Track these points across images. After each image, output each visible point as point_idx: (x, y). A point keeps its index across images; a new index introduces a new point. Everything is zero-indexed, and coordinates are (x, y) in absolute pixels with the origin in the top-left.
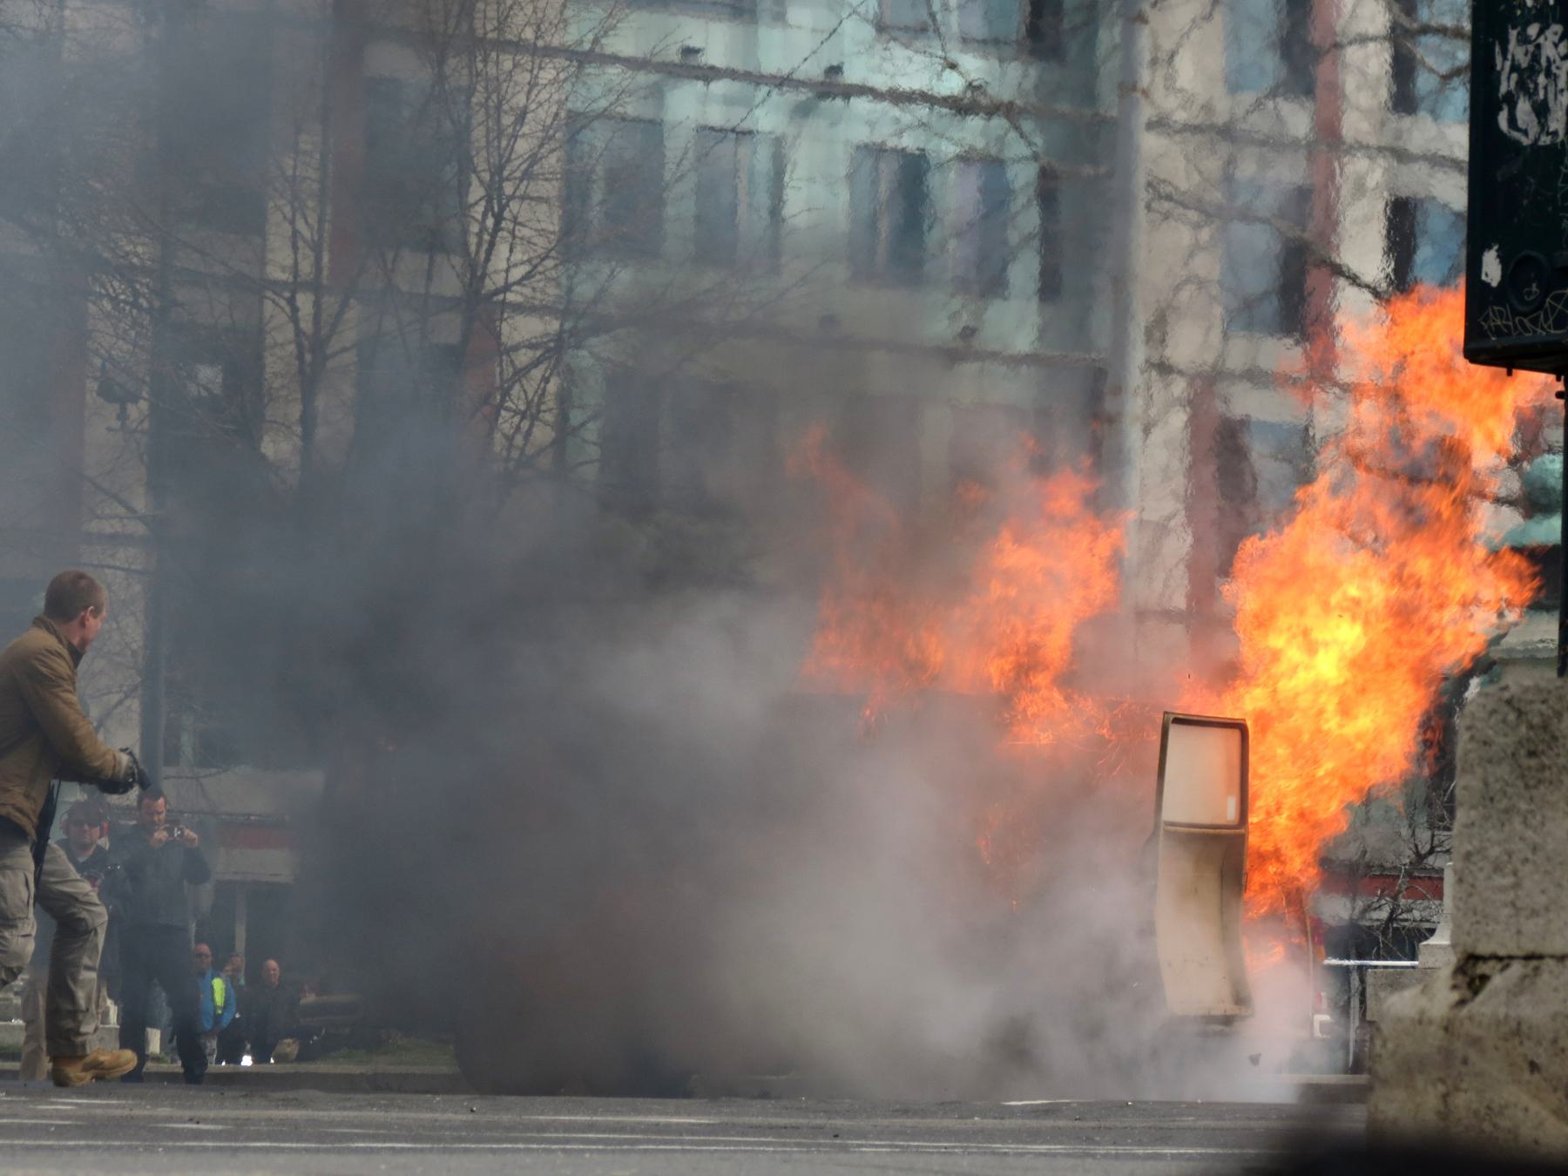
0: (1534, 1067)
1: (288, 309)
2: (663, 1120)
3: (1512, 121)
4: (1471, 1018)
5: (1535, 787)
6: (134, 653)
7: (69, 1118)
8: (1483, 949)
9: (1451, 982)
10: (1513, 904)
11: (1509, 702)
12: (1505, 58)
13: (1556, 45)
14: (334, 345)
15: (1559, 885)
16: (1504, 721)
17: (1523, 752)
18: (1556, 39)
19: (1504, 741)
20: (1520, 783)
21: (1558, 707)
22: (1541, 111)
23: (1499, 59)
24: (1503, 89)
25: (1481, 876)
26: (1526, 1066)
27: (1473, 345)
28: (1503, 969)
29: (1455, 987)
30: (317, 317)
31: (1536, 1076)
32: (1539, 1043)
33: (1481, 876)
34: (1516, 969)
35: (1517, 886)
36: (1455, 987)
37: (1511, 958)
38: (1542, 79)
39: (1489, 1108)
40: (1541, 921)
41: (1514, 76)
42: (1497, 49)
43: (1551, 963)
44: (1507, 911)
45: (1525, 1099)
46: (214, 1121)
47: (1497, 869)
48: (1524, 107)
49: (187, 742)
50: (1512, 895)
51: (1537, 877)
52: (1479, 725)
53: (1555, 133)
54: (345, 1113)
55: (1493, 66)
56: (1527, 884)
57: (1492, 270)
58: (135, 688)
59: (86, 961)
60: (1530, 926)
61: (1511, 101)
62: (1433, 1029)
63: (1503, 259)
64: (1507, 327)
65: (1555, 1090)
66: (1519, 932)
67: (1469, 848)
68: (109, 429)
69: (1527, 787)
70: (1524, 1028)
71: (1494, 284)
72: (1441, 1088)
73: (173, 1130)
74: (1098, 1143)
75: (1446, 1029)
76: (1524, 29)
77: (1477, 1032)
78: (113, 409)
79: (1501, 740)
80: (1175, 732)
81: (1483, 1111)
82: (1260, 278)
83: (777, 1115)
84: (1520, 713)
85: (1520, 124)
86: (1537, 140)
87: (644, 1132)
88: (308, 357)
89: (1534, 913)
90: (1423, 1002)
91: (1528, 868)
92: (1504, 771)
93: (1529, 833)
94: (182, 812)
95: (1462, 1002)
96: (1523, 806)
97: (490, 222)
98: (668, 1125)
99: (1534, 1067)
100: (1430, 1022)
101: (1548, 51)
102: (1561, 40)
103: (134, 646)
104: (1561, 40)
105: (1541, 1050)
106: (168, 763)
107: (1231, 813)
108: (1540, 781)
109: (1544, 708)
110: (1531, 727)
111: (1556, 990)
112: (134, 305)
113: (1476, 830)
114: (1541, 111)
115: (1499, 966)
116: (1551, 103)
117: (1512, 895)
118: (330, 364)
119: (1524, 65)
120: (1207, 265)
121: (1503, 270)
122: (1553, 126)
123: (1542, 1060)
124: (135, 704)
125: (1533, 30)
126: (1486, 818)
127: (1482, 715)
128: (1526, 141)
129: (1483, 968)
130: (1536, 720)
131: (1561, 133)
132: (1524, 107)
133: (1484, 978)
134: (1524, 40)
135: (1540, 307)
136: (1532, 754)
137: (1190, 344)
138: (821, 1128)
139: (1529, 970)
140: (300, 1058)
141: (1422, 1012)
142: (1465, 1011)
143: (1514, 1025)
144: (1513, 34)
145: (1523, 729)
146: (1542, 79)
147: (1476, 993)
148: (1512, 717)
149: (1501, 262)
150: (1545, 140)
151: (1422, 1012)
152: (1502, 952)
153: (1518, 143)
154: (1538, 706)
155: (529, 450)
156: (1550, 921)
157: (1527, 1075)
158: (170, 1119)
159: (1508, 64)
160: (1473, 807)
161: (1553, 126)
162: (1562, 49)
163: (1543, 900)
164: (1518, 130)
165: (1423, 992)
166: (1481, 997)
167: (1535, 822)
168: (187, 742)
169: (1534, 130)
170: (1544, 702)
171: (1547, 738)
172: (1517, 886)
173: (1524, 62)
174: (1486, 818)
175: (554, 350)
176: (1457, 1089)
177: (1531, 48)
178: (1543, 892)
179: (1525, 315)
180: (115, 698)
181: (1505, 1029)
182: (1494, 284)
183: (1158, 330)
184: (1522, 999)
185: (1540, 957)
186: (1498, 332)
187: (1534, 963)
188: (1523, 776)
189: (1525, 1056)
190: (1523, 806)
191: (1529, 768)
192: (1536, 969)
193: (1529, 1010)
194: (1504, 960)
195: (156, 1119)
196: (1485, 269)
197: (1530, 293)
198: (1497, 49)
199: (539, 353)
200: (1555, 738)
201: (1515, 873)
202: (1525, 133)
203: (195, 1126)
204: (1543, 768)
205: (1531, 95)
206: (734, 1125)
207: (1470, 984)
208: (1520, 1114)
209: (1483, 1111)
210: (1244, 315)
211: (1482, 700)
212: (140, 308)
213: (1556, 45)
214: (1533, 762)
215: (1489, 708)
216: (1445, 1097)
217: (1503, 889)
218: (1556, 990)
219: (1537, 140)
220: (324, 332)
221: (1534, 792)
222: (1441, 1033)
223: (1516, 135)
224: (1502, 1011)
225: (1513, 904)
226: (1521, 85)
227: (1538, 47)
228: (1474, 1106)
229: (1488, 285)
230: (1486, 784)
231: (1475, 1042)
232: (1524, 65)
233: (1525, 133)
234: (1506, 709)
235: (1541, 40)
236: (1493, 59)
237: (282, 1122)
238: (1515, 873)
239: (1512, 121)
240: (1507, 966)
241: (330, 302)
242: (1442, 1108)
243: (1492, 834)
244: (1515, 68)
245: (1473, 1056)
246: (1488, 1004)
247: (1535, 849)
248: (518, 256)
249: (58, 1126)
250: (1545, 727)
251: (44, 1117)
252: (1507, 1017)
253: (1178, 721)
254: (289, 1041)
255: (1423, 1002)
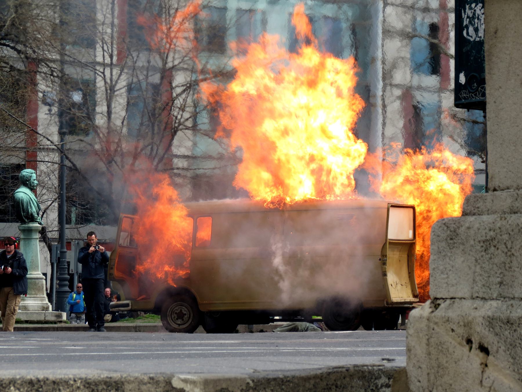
0: (453, 330)
1: (102, 76)
2: (223, 342)
3: (468, 33)
4: (435, 316)
5: (452, 249)
6: (55, 188)
7: (34, 346)
8: (439, 296)
9: (430, 306)
10: (447, 283)
11: (444, 224)
12: (465, 14)
13: (480, 10)
14: (117, 88)
15: (460, 277)
16: (443, 230)
17: (449, 239)
18: (480, 8)
19: (443, 236)
20: (448, 248)
21: (458, 225)
22: (476, 30)
23: (463, 14)
24: (465, 24)
25: (438, 275)
26: (450, 330)
27: (457, 103)
28: (444, 302)
29: (430, 307)
30: (111, 80)
31: (454, 333)
32: (454, 324)
33: (438, 275)
34: (448, 302)
35: (448, 277)
36: (430, 307)
37: (447, 298)
38: (476, 20)
39: (440, 342)
40: (455, 288)
41: (468, 20)
42: (463, 11)
43: (458, 300)
44: (445, 285)
45: (450, 340)
46: (80, 346)
47: (442, 273)
48: (471, 29)
49: (73, 216)
50: (446, 280)
51: (453, 275)
52: (436, 231)
53: (481, 37)
54: (122, 342)
55: (462, 16)
56: (451, 277)
57: (462, 79)
58: (56, 199)
59: (125, 94)
60: (452, 289)
61: (467, 27)
62: (424, 320)
63: (466, 76)
64: (467, 97)
65: (459, 337)
66: (449, 291)
67: (434, 266)
68: (46, 114)
69: (450, 249)
70: (450, 319)
71: (463, 84)
72: (427, 337)
73: (67, 349)
74: (359, 347)
75: (428, 320)
76: (471, 5)
77: (437, 320)
78: (47, 108)
79: (442, 235)
80: (392, 210)
81: (439, 344)
82: (424, 54)
83: (261, 339)
84: (448, 227)
85: (470, 34)
86: (475, 39)
87: (216, 346)
88: (109, 91)
89: (453, 285)
90: (421, 312)
91: (451, 272)
92: (443, 244)
93: (451, 262)
94: (72, 239)
95: (432, 312)
96: (449, 254)
97: (168, 46)
98: (225, 343)
99: (453, 330)
100: (423, 318)
101: (478, 12)
102: (482, 8)
103: (56, 186)
104: (482, 8)
105: (454, 326)
106: (67, 224)
107: (410, 235)
108: (454, 247)
109: (454, 225)
110: (451, 231)
111: (459, 308)
112: (52, 75)
113: (436, 261)
114: (476, 30)
115: (443, 301)
116: (479, 28)
117: (446, 280)
118: (116, 93)
119: (471, 16)
120: (406, 53)
121: (466, 79)
122: (480, 35)
123: (455, 329)
124: (56, 204)
125: (473, 5)
126: (439, 258)
127: (437, 228)
128: (472, 40)
129: (439, 302)
130: (452, 229)
131: (482, 37)
132: (471, 29)
133: (439, 305)
134: (471, 8)
135: (477, 90)
136: (451, 239)
137: (402, 76)
138: (273, 343)
139: (452, 302)
140: (113, 321)
141: (421, 315)
142: (433, 314)
143: (447, 318)
144: (467, 7)
145: (449, 232)
146: (476, 20)
147: (437, 309)
148: (445, 228)
149: (465, 77)
150: (478, 39)
151: (421, 315)
152: (444, 297)
153: (470, 40)
154: (453, 225)
155: (182, 120)
156: (457, 288)
157: (451, 333)
158: (66, 345)
159: (466, 16)
160: (435, 255)
161: (480, 35)
162: (482, 11)
163: (455, 282)
164: (470, 36)
165: (422, 309)
166: (438, 310)
167: (453, 259)
168: (73, 216)
169: (474, 36)
170: (454, 224)
171: (455, 234)
172: (448, 277)
173: (471, 15)
174: (439, 258)
175: (191, 87)
176: (431, 337)
177: (473, 11)
178: (455, 279)
179: (473, 93)
180: (50, 203)
181: (444, 320)
182: (463, 84)
183: (387, 76)
184: (450, 311)
185: (455, 298)
186: (465, 98)
187: (453, 300)
188: (449, 246)
189: (450, 327)
190: (449, 254)
191: (451, 243)
192: (454, 302)
193: (451, 314)
194: (444, 299)
195: (62, 345)
196: (460, 79)
197: (474, 86)
198: (463, 11)
199: (185, 87)
200: (458, 234)
201: (447, 274)
202: (472, 37)
203: (74, 348)
204: (454, 243)
205: (473, 25)
206: (246, 343)
207: (435, 307)
208: (449, 344)
209: (439, 344)
210: (417, 68)
211: (437, 224)
212: (54, 76)
213: (480, 10)
214: (451, 241)
215: (439, 225)
216: (428, 340)
217: (444, 279)
218: (459, 308)
219: (475, 39)
220: (114, 83)
221: (452, 250)
222: (427, 321)
223: (469, 38)
224: (443, 314)
225: (447, 283)
226: (470, 22)
227: (475, 10)
228: (436, 342)
229: (461, 84)
230: (439, 248)
231: (436, 323)
232: (471, 16)
233: (472, 37)
234: (444, 226)
235: (476, 8)
236: (461, 14)
237: (102, 345)
238: (447, 274)
239: (468, 33)
240: (445, 301)
241: (116, 71)
242: (427, 342)
243: (440, 262)
244: (468, 17)
245: (436, 328)
246: (439, 313)
247: (452, 267)
248: (177, 56)
249: (30, 349)
250: (455, 231)
251: (26, 346)
252: (445, 316)
253: (392, 206)
254: (108, 315)
255: (421, 312)
